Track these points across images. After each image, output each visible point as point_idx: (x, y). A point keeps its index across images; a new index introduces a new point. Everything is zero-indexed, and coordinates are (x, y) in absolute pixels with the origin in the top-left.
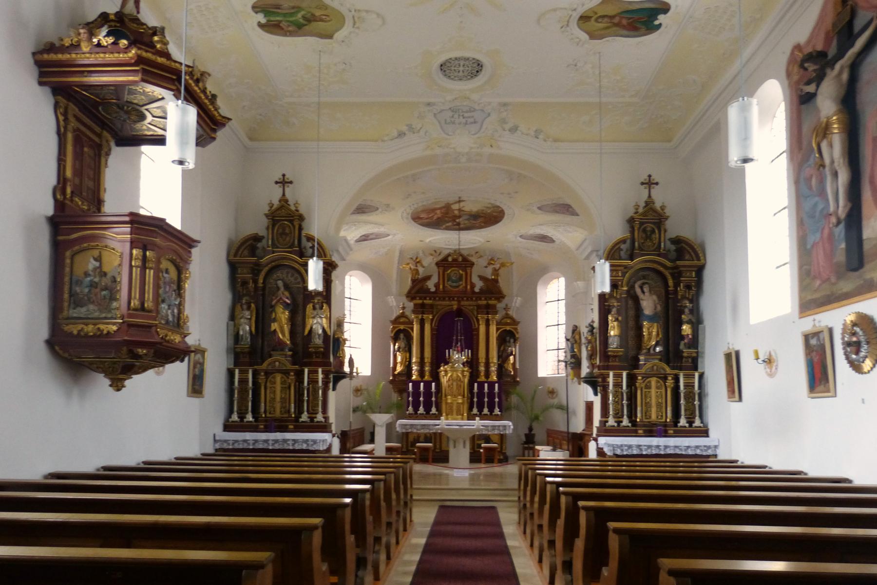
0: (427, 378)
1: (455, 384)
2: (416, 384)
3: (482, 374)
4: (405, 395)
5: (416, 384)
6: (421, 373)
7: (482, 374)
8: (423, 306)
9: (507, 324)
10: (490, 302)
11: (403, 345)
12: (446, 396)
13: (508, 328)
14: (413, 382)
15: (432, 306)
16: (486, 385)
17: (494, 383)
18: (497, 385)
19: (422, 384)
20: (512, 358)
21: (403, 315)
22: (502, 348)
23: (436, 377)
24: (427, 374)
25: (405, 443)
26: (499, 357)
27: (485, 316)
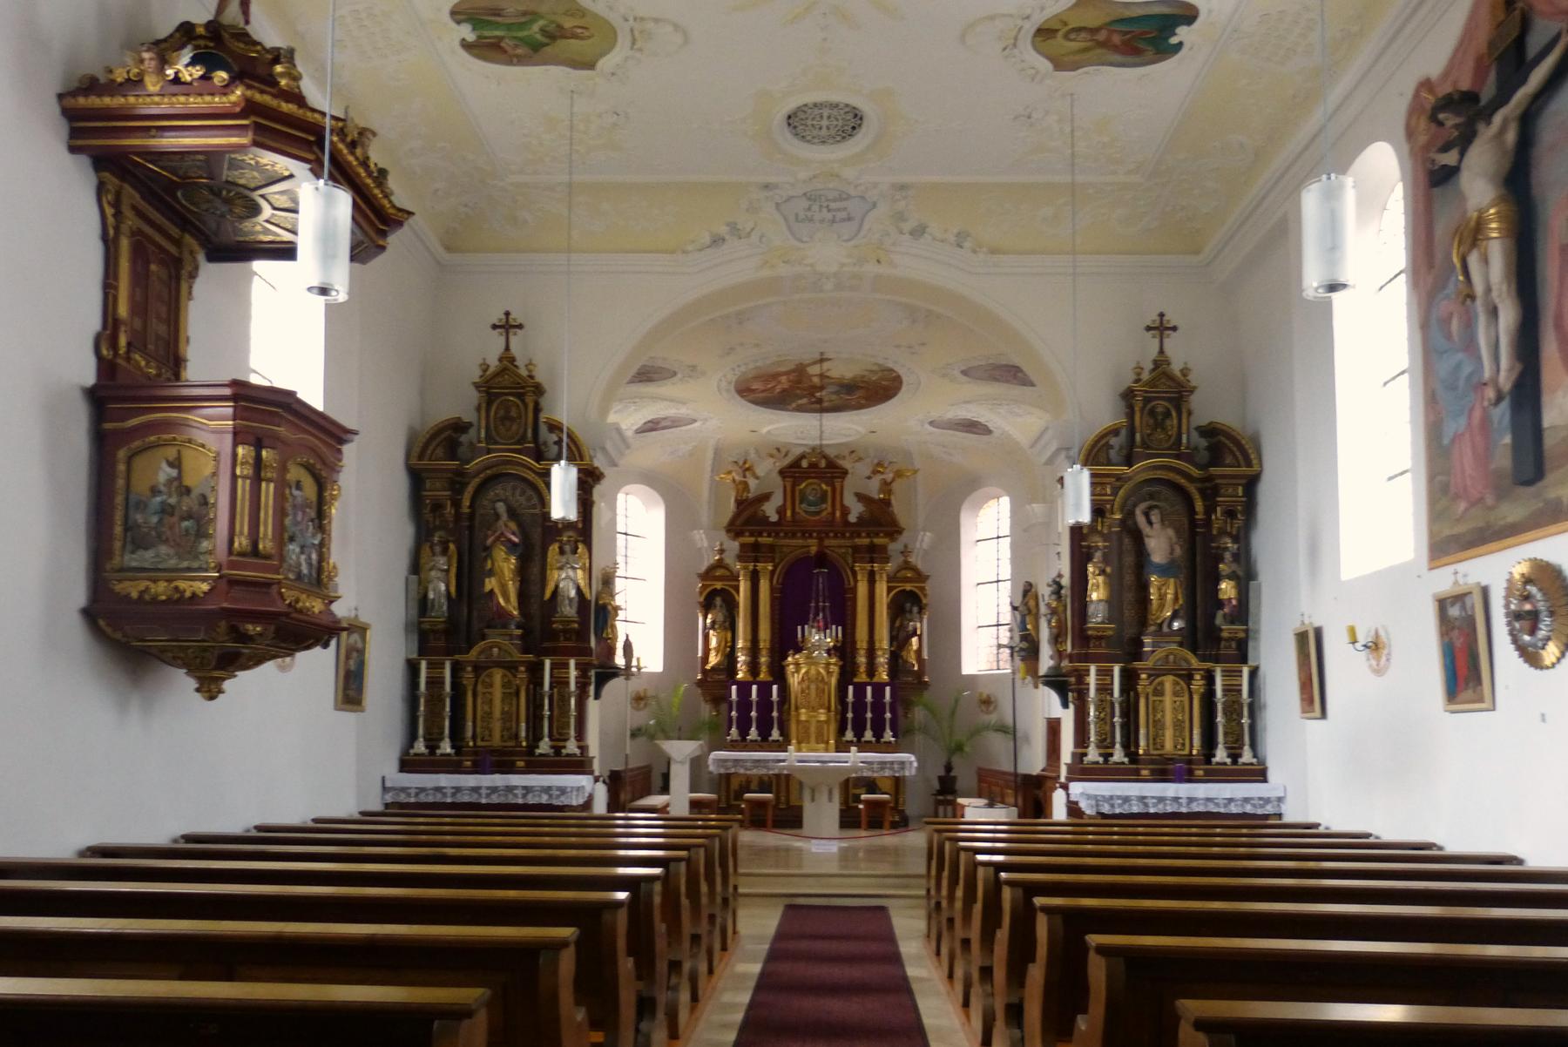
0: (763, 676)
1: (813, 687)
2: (744, 688)
3: (862, 669)
4: (724, 707)
5: (744, 688)
6: (753, 667)
7: (862, 669)
8: (756, 547)
9: (907, 580)
10: (876, 541)
11: (720, 618)
12: (797, 708)
13: (908, 587)
14: (739, 683)
15: (772, 548)
16: (869, 689)
17: (883, 685)
18: (888, 689)
19: (754, 687)
20: (915, 640)
21: (720, 564)
22: (897, 624)
23: (779, 675)
24: (764, 669)
25: (724, 793)
26: (893, 639)
27: (868, 566)
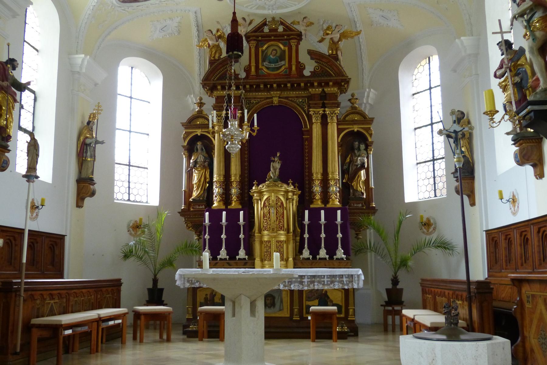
0: (234, 205)
2: (216, 215)
3: (318, 197)
5: (216, 215)
6: (226, 198)
7: (318, 197)
9: (354, 122)
11: (201, 159)
12: (260, 231)
13: (356, 128)
19: (224, 213)
20: (363, 172)
21: (200, 115)
22: (348, 160)
23: (247, 203)
26: (344, 172)
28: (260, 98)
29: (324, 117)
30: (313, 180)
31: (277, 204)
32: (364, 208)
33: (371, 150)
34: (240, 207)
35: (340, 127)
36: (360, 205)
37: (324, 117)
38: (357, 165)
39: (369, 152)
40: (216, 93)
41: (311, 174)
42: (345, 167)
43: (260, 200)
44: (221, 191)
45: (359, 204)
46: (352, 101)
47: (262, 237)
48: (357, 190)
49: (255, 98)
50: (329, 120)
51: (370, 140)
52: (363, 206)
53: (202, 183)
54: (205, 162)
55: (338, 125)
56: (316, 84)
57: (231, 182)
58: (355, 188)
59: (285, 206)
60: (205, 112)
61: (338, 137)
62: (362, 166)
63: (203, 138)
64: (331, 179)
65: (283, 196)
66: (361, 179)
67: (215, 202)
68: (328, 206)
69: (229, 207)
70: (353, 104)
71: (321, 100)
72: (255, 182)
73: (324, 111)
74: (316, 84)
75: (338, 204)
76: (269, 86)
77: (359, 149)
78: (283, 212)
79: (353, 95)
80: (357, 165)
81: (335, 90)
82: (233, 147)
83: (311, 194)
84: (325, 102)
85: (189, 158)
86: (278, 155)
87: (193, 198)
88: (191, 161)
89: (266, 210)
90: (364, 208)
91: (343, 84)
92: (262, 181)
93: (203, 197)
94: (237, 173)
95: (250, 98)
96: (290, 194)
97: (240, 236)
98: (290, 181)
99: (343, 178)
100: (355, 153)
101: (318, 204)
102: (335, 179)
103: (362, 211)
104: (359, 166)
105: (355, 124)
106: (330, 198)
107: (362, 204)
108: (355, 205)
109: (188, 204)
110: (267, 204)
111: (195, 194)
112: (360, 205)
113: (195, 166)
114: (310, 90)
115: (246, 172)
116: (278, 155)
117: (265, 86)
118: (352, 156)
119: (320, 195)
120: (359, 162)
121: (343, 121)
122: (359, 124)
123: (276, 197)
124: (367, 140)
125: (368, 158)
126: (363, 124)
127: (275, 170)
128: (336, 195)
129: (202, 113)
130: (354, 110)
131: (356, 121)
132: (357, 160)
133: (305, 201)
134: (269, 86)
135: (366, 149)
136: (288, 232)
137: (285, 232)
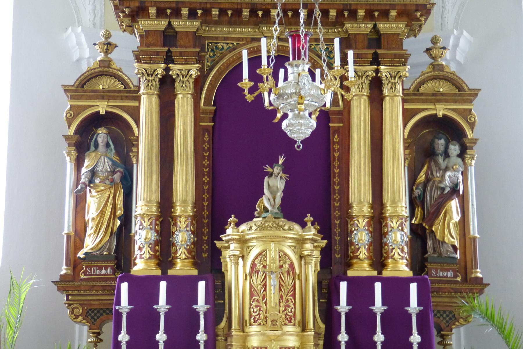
0: (182, 267)
1: (273, 282)
2: (143, 289)
3: (363, 253)
4: (108, 328)
5: (143, 289)
6: (164, 253)
7: (363, 253)
8: (169, 37)
9: (436, 97)
10: (383, 27)
11: (105, 165)
12: (243, 325)
13: (440, 110)
14: (353, 283)
15: (197, 39)
16: (378, 286)
17: (405, 282)
18: (413, 287)
19: (163, 285)
20: (454, 204)
21: (105, 70)
22: (422, 177)
23: (210, 263)
24: (182, 253)
25: (211, 161)
26: (414, 203)
27: (370, 70)
28: (238, 39)
29: (376, 84)
30: (352, 217)
31: (281, 267)
32: (459, 279)
33: (473, 158)
34: (195, 272)
35: (407, 106)
36: (451, 274)
37: (376, 84)
38: (443, 189)
39: (468, 161)
40: (143, 24)
41: (347, 206)
42: (417, 192)
43: (243, 257)
44: (152, 236)
45: (448, 270)
46: (434, 52)
47: (245, 338)
48: (444, 242)
49: (226, 39)
50: (386, 92)
51: (470, 135)
52: (456, 276)
53: (106, 218)
54: (113, 172)
55: (404, 101)
56: (361, 13)
57: (174, 218)
58: (438, 236)
59: (297, 271)
60: (116, 65)
61: (405, 126)
62: (454, 190)
63: (109, 119)
64: (392, 217)
65: (294, 249)
66: (451, 218)
67: (138, 261)
68: (387, 273)
69: (170, 272)
70: (434, 58)
71: (369, 47)
72: (232, 219)
73: (377, 71)
74: (361, 13)
75: (407, 269)
76: (260, 13)
77: (446, 155)
78: (294, 285)
79: (434, 41)
80: (443, 189)
81: (400, 27)
82: (300, 125)
83: (347, 244)
84: (379, 51)
85: (79, 163)
86: (281, 161)
87: (85, 250)
88: (84, 170)
89: (257, 280)
90: (459, 279)
91: (418, 14)
92: (245, 216)
93: (109, 250)
94: (189, 198)
95: (216, 38)
96: (308, 246)
97: (198, 337)
98: (309, 218)
99: (412, 214)
100: (437, 163)
101: (362, 269)
102: (399, 217)
103: (454, 286)
104: (447, 190)
105: (439, 101)
106: (387, 258)
107: (454, 271)
108: (440, 274)
109: (75, 264)
110: (259, 267)
111: (90, 243)
112: (451, 274)
113: (91, 181)
114: (348, 25)
115: (206, 196)
116: (281, 161)
117: (253, 12)
118: (429, 167)
119: (368, 250)
120: (447, 182)
121: (415, 95)
122: (447, 101)
123: (280, 251)
124: (464, 135)
125: (464, 174)
126: (455, 102)
127: (274, 194)
128: (402, 251)
129: (109, 67)
130: (438, 73)
131: (442, 94)
132: (443, 177)
133: (334, 261)
134: (260, 13)
135: (462, 155)
136: (304, 328)
137: (299, 329)
